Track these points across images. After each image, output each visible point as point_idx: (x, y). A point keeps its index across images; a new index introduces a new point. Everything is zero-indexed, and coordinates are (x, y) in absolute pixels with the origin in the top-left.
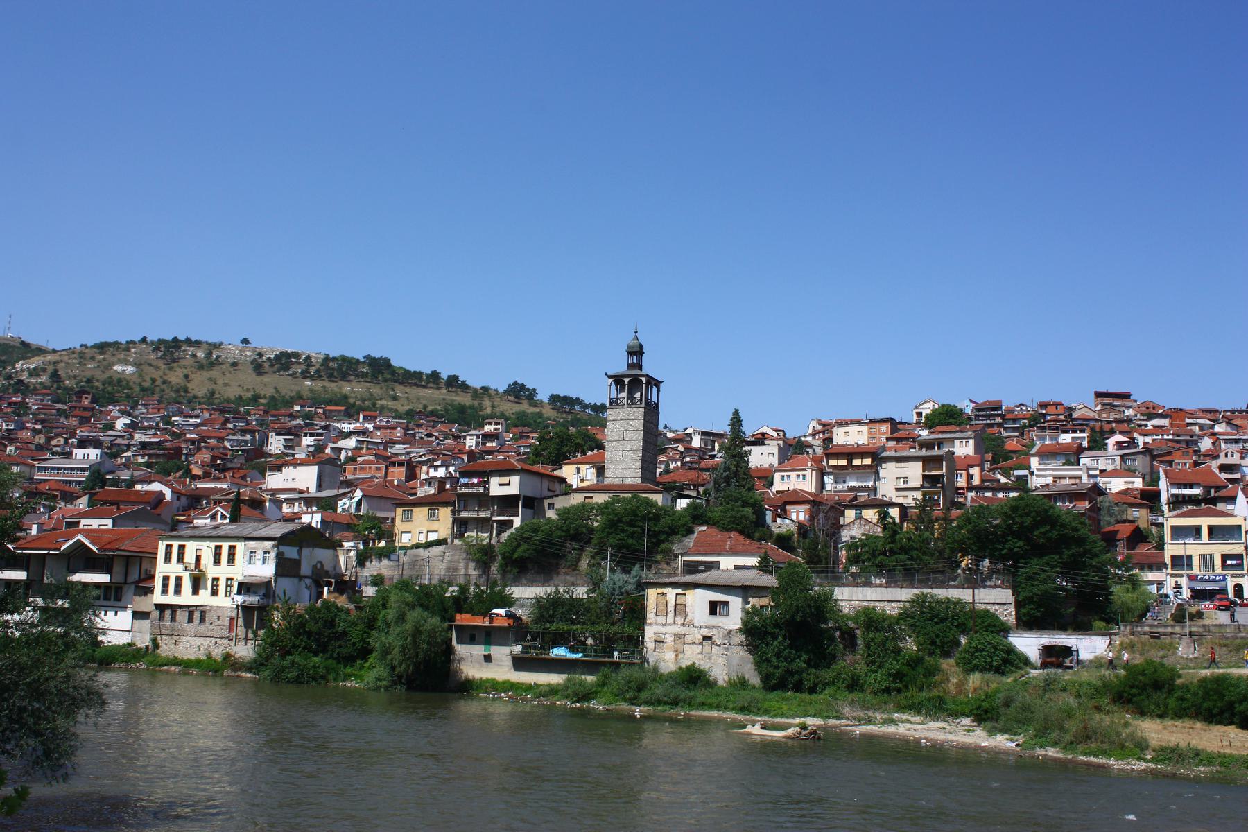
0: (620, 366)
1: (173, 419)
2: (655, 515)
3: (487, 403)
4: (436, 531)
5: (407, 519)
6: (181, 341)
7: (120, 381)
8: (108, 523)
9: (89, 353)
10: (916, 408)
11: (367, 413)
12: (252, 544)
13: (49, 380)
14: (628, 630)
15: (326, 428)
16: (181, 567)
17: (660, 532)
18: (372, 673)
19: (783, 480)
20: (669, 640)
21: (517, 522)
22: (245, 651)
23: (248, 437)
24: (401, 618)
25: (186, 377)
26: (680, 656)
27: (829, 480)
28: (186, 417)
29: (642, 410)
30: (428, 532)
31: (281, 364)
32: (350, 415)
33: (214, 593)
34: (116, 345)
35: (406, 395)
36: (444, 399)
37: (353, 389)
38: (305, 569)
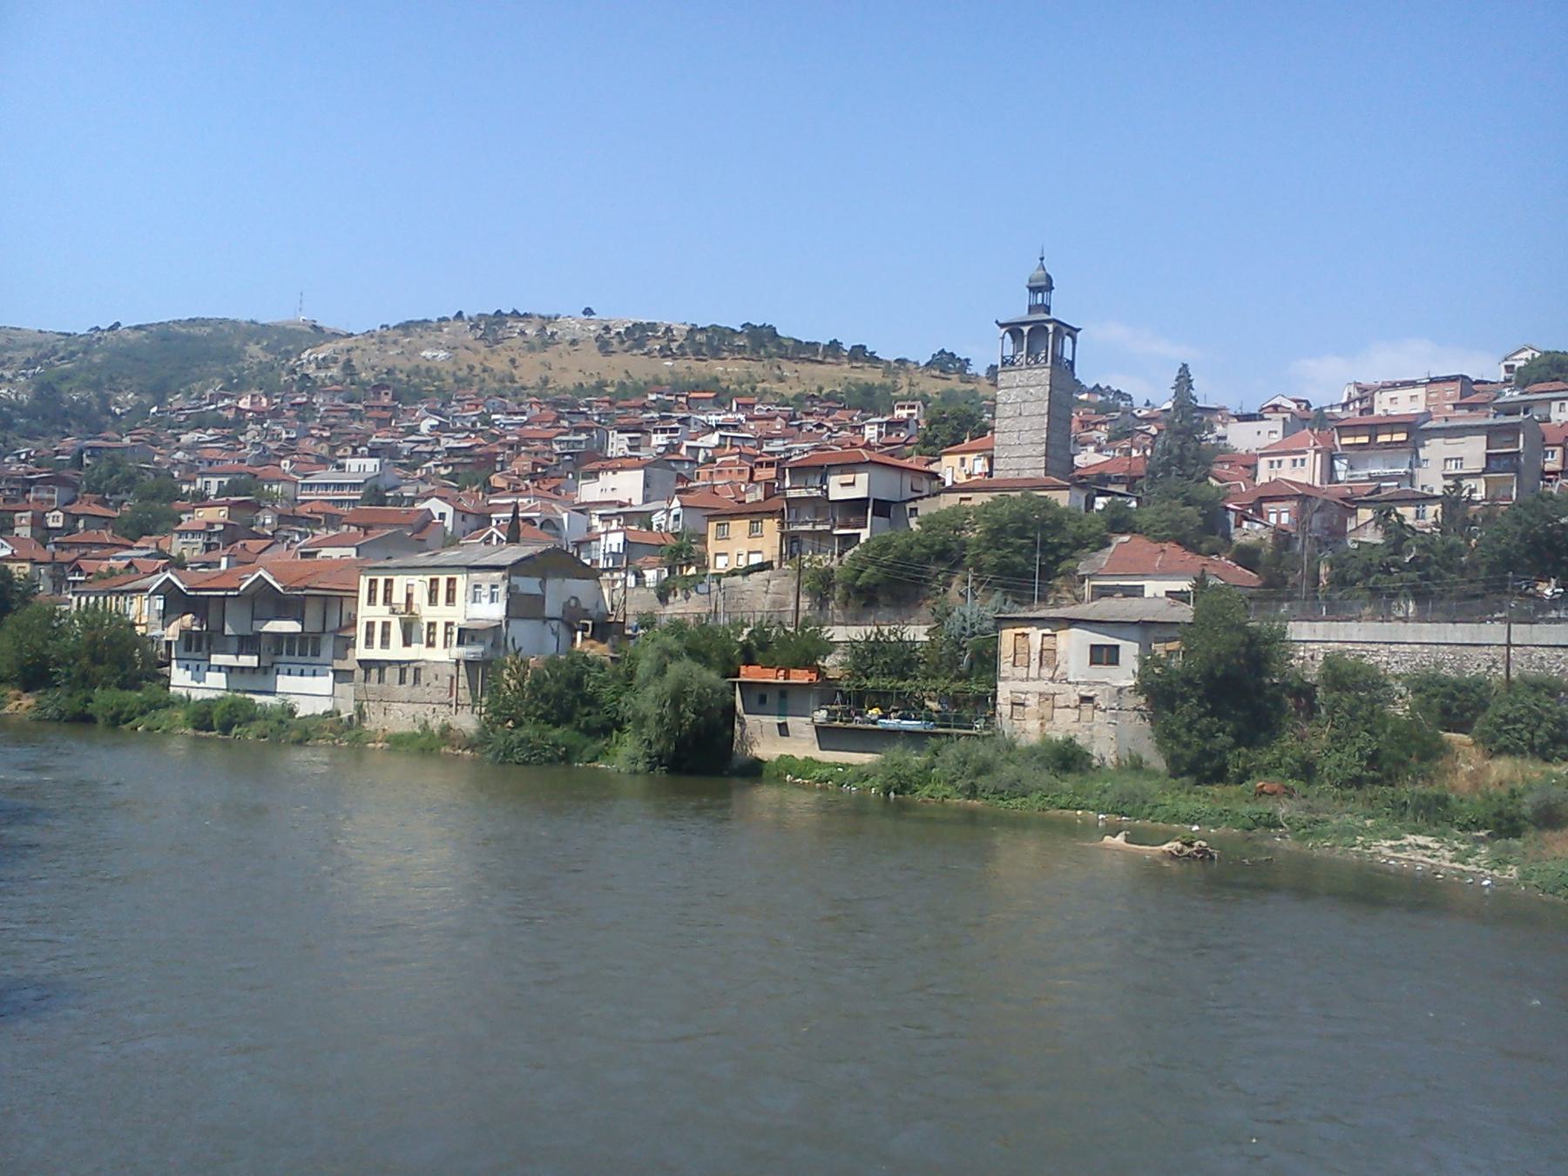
0: (1018, 310)
1: (494, 417)
2: (1056, 521)
3: (903, 381)
4: (760, 552)
5: (723, 537)
6: (506, 315)
7: (428, 370)
8: (352, 552)
9: (392, 336)
10: (1506, 359)
11: (741, 400)
12: (476, 576)
13: (342, 373)
14: (976, 688)
15: (683, 421)
16: (387, 608)
17: (1061, 545)
18: (626, 752)
19: (1295, 465)
20: (1032, 701)
21: (865, 534)
22: (467, 722)
23: (583, 436)
24: (661, 671)
25: (513, 361)
26: (1048, 726)
27: (1340, 465)
28: (509, 414)
29: (1048, 371)
30: (749, 553)
31: (635, 340)
32: (720, 402)
33: (431, 644)
34: (425, 323)
35: (796, 374)
36: (846, 378)
37: (728, 369)
38: (552, 607)
